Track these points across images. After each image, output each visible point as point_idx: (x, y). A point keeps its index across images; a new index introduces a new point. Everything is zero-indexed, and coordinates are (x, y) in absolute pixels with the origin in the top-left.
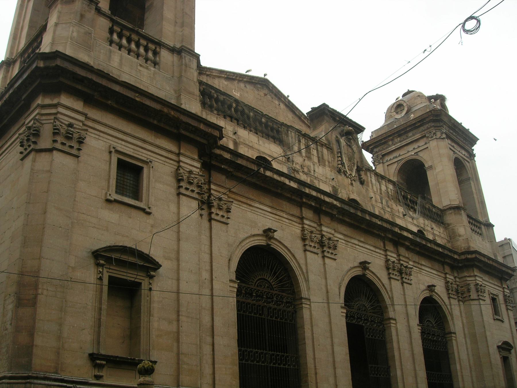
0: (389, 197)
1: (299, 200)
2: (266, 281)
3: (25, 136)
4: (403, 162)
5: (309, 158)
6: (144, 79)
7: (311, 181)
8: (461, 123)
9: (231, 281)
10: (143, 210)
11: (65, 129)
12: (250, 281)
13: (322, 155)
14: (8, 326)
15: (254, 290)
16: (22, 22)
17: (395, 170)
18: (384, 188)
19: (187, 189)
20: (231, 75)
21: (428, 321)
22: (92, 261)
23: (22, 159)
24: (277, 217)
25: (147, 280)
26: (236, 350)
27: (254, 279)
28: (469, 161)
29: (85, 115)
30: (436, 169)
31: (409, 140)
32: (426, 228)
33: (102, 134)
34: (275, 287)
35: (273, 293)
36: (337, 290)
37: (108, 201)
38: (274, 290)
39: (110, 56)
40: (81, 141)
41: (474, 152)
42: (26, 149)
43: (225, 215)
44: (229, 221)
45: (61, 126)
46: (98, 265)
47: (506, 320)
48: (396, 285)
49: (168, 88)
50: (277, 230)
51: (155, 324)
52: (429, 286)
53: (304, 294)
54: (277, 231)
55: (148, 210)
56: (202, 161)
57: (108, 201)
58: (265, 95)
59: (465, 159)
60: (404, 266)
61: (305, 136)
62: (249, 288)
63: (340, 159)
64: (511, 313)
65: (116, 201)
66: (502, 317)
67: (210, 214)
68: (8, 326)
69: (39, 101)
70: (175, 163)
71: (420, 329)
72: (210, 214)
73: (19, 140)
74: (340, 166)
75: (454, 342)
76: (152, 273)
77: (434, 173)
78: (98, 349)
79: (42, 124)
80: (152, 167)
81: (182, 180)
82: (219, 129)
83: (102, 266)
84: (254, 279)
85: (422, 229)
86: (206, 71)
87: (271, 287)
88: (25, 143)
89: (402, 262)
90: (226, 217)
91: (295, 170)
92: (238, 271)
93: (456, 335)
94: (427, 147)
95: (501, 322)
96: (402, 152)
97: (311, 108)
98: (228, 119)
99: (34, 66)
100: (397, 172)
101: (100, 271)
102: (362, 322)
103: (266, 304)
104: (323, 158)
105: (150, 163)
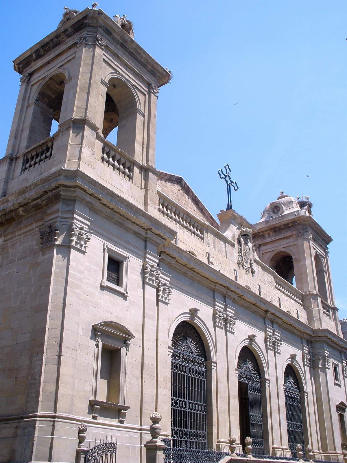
4: (275, 252)
8: (127, 27)
12: (179, 347)
15: (181, 354)
16: (22, 125)
17: (268, 258)
21: (289, 381)
27: (181, 345)
28: (324, 257)
30: (300, 261)
31: (282, 236)
35: (186, 355)
37: (103, 288)
38: (193, 354)
44: (170, 302)
45: (76, 228)
48: (220, 332)
50: (200, 309)
54: (200, 310)
59: (137, 88)
60: (229, 316)
66: (340, 383)
74: (240, 259)
75: (306, 399)
77: (299, 265)
78: (95, 397)
80: (130, 261)
82: (173, 234)
84: (181, 345)
87: (191, 352)
89: (227, 312)
93: (307, 394)
94: (296, 244)
96: (274, 245)
100: (269, 260)
102: (199, 366)
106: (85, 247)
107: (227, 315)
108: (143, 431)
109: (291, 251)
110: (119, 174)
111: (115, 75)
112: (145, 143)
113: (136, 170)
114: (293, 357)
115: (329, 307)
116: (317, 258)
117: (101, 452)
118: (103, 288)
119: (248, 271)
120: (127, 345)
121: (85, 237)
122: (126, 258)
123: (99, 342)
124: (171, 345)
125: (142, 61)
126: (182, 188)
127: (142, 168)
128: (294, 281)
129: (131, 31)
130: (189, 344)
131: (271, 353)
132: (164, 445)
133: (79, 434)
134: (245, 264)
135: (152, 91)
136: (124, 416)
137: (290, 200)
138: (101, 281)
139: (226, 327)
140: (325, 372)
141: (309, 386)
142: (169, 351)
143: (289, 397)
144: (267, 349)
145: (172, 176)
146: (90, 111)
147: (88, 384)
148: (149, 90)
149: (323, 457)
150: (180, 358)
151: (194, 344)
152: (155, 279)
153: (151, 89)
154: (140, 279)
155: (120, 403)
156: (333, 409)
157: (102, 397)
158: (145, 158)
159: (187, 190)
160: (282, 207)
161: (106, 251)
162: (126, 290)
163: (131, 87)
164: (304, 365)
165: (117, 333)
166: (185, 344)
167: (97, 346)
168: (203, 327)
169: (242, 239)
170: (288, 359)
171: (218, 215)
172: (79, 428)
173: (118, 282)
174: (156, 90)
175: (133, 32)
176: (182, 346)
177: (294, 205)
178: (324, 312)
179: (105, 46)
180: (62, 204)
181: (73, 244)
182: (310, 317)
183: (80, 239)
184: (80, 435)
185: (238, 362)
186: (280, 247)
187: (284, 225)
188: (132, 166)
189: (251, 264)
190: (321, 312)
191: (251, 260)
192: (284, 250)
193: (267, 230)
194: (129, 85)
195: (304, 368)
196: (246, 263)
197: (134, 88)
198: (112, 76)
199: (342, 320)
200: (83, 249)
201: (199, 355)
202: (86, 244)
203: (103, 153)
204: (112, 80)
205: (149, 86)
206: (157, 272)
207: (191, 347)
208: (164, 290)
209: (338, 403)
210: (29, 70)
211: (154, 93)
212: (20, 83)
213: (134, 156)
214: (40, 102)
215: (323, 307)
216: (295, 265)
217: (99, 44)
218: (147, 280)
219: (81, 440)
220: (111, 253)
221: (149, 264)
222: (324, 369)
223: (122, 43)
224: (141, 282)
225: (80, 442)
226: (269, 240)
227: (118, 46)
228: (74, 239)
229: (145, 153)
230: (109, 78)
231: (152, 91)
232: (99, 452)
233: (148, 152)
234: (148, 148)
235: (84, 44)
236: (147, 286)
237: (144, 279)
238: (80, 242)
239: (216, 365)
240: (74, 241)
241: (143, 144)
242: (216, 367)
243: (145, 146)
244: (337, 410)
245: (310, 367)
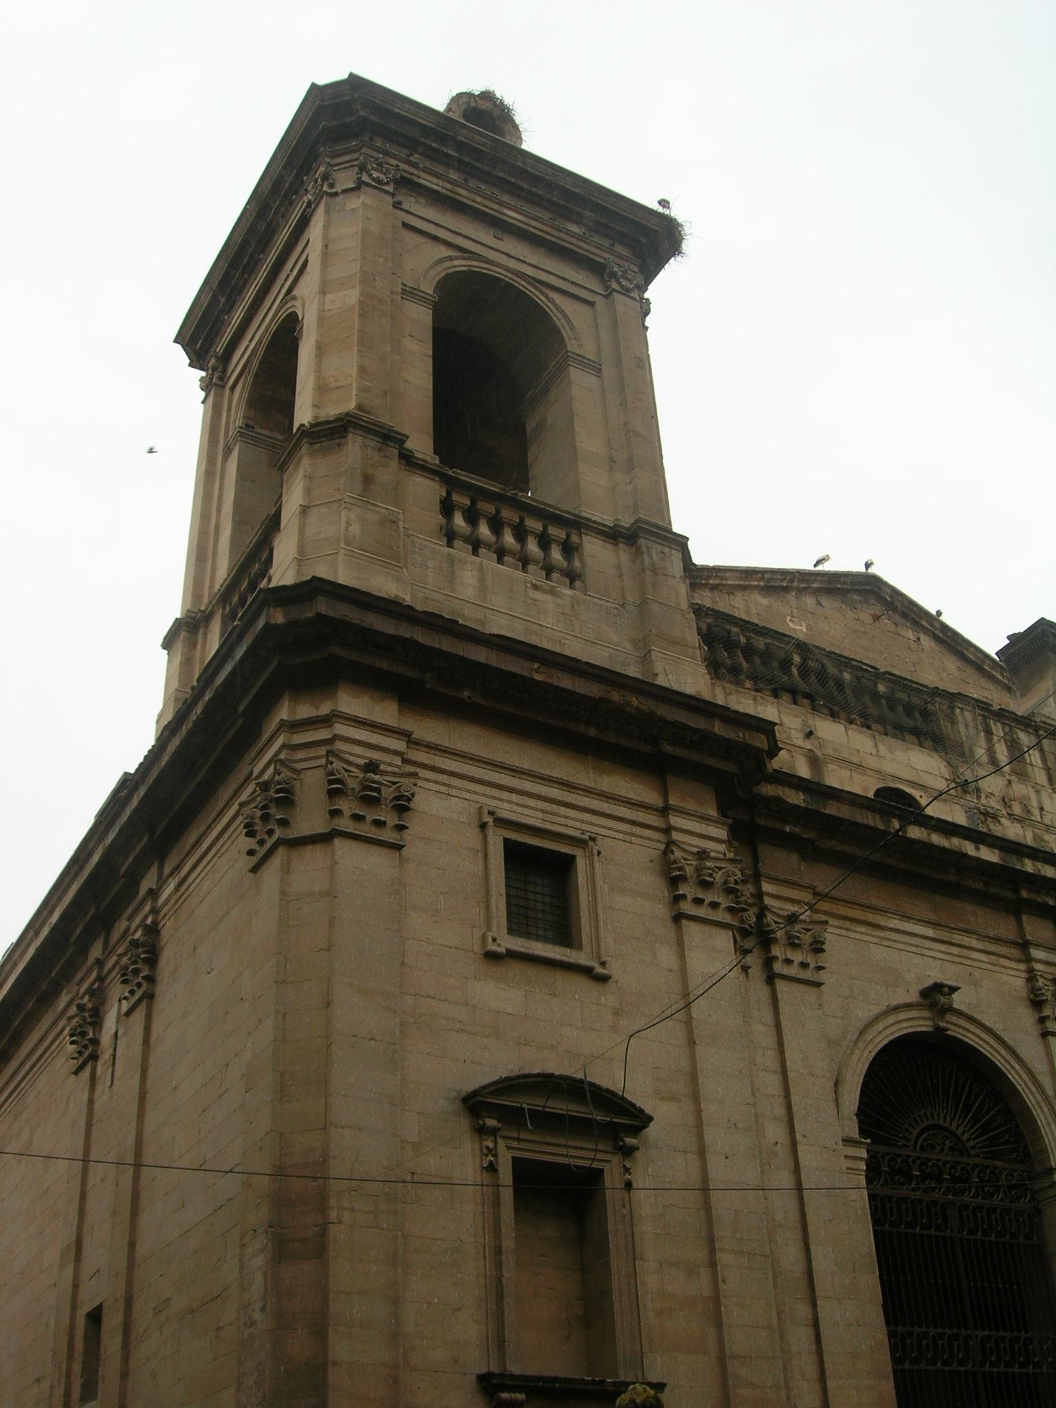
1: (1011, 895)
2: (945, 1133)
3: (256, 807)
5: (1023, 776)
6: (548, 622)
7: (1035, 837)
9: (848, 1141)
10: (587, 971)
11: (358, 777)
14: (257, 1315)
15: (883, 1157)
19: (698, 902)
20: (777, 579)
22: (465, 1124)
23: (255, 870)
25: (616, 1160)
26: (880, 1333)
27: (910, 1129)
29: (407, 736)
33: (456, 782)
34: (973, 1147)
35: (968, 1164)
38: (969, 1155)
39: (453, 573)
40: (402, 806)
42: (261, 842)
43: (810, 960)
46: (481, 1131)
49: (615, 639)
50: (959, 985)
55: (600, 970)
57: (492, 957)
61: (1002, 715)
62: (899, 1156)
65: (512, 955)
67: (769, 962)
68: (257, 1315)
69: (284, 712)
72: (769, 962)
73: (240, 818)
76: (629, 1141)
79: (298, 772)
80: (599, 853)
81: (683, 878)
82: (766, 728)
83: (493, 1132)
86: (709, 577)
88: (259, 826)
90: (812, 966)
92: (861, 1114)
98: (786, 697)
99: (260, 624)
101: (487, 1147)
103: (954, 1195)
105: (591, 843)
123: (495, 1156)
125: (554, 199)
130: (933, 1118)
142: (846, 1157)
150: (941, 1181)
151: (966, 1117)
163: (531, 291)
166: (922, 1126)
168: (990, 1049)
171: (997, 654)
173: (565, 933)
174: (629, 280)
176: (916, 1132)
180: (289, 700)
194: (522, 285)
197: (536, 288)
198: (449, 271)
210: (220, 346)
212: (202, 394)
214: (258, 430)
217: (622, 287)
230: (438, 279)
235: (325, 197)
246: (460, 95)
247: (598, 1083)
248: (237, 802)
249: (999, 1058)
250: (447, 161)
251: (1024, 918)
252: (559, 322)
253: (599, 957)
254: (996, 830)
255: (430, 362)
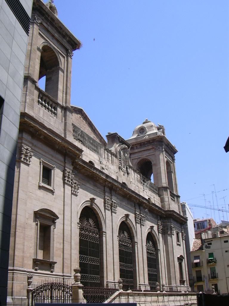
0: (137, 181)
5: (108, 161)
6: (52, 123)
13: (113, 160)
18: (136, 176)
24: (95, 192)
30: (157, 166)
32: (151, 197)
33: (38, 153)
36: (116, 228)
39: (40, 111)
41: (175, 158)
44: (117, 212)
47: (182, 245)
48: (108, 213)
49: (60, 128)
51: (55, 245)
52: (151, 227)
53: (104, 230)
56: (73, 167)
58: (80, 117)
59: (59, 52)
63: (120, 162)
64: (184, 241)
70: (63, 167)
71: (79, 226)
72: (112, 209)
74: (120, 165)
75: (159, 254)
78: (37, 257)
82: (81, 151)
85: (150, 198)
89: (113, 200)
91: (103, 168)
95: (50, 194)
96: (140, 154)
97: (108, 133)
98: (78, 141)
100: (137, 163)
104: (113, 162)
106: (30, 161)
107: (112, 201)
108: (65, 277)
109: (151, 159)
110: (39, 104)
111: (46, 44)
112: (65, 91)
113: (59, 110)
114: (152, 227)
115: (174, 195)
116: (168, 164)
117: (43, 289)
118: (40, 187)
119: (125, 173)
120: (54, 223)
121: (29, 155)
122: (54, 168)
124: (79, 222)
126: (82, 116)
127: (62, 107)
128: (152, 177)
129: (56, 11)
131: (138, 225)
132: (82, 285)
133: (28, 280)
134: (123, 168)
135: (69, 55)
136: (53, 268)
137: (151, 125)
138: (39, 183)
139: (112, 209)
140: (172, 237)
141: (161, 246)
143: (149, 253)
144: (136, 223)
145: (76, 108)
146: (31, 70)
147: (32, 248)
148: (67, 54)
149: (168, 289)
152: (70, 181)
153: (68, 54)
154: (62, 181)
155: (51, 260)
156: (176, 260)
157: (40, 256)
158: (64, 101)
159: (85, 118)
160: (146, 129)
161: (41, 163)
162: (53, 188)
163: (56, 52)
164: (159, 232)
165: (48, 215)
167: (37, 224)
169: (122, 152)
170: (122, 217)
172: (28, 277)
173: (49, 184)
175: (57, 12)
177: (154, 128)
178: (171, 199)
179: (40, 23)
181: (22, 159)
182: (162, 201)
183: (26, 156)
184: (29, 280)
185: (119, 231)
186: (144, 155)
187: (147, 141)
188: (56, 106)
189: (127, 168)
190: (170, 199)
191: (127, 166)
192: (146, 158)
193: (136, 144)
195: (159, 235)
196: (124, 167)
197: (57, 53)
199: (182, 203)
200: (28, 162)
201: (95, 228)
202: (30, 159)
203: (39, 98)
204: (44, 47)
205: (67, 50)
206: (72, 176)
207: (91, 223)
208: (75, 186)
209: (179, 256)
211: (71, 56)
213: (57, 99)
215: (171, 195)
216: (153, 168)
217: (37, 22)
218: (66, 181)
219: (29, 284)
220: (44, 164)
221: (67, 171)
222: (171, 234)
223: (50, 21)
224: (62, 184)
225: (28, 285)
226: (136, 151)
227: (48, 24)
228: (23, 156)
229: (64, 98)
231: (69, 55)
232: (41, 290)
233: (66, 97)
234: (66, 94)
236: (66, 186)
237: (64, 180)
238: (26, 158)
239: (105, 234)
240: (23, 158)
241: (63, 91)
242: (106, 235)
243: (65, 93)
244: (178, 260)
245: (162, 234)
246: (79, 48)
247: (52, 210)
248: (92, 196)
249: (99, 212)
250: (48, 20)
251: (112, 191)
252: (59, 60)
253: (54, 188)
254: (104, 171)
255: (39, 64)
